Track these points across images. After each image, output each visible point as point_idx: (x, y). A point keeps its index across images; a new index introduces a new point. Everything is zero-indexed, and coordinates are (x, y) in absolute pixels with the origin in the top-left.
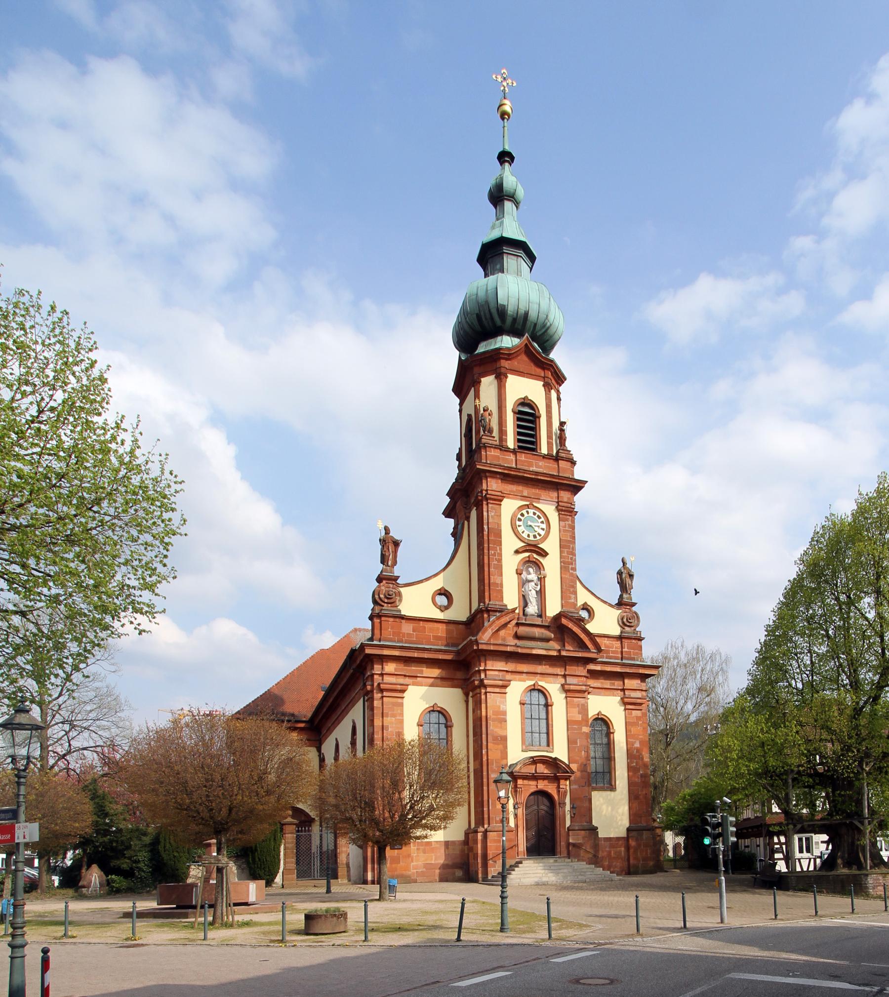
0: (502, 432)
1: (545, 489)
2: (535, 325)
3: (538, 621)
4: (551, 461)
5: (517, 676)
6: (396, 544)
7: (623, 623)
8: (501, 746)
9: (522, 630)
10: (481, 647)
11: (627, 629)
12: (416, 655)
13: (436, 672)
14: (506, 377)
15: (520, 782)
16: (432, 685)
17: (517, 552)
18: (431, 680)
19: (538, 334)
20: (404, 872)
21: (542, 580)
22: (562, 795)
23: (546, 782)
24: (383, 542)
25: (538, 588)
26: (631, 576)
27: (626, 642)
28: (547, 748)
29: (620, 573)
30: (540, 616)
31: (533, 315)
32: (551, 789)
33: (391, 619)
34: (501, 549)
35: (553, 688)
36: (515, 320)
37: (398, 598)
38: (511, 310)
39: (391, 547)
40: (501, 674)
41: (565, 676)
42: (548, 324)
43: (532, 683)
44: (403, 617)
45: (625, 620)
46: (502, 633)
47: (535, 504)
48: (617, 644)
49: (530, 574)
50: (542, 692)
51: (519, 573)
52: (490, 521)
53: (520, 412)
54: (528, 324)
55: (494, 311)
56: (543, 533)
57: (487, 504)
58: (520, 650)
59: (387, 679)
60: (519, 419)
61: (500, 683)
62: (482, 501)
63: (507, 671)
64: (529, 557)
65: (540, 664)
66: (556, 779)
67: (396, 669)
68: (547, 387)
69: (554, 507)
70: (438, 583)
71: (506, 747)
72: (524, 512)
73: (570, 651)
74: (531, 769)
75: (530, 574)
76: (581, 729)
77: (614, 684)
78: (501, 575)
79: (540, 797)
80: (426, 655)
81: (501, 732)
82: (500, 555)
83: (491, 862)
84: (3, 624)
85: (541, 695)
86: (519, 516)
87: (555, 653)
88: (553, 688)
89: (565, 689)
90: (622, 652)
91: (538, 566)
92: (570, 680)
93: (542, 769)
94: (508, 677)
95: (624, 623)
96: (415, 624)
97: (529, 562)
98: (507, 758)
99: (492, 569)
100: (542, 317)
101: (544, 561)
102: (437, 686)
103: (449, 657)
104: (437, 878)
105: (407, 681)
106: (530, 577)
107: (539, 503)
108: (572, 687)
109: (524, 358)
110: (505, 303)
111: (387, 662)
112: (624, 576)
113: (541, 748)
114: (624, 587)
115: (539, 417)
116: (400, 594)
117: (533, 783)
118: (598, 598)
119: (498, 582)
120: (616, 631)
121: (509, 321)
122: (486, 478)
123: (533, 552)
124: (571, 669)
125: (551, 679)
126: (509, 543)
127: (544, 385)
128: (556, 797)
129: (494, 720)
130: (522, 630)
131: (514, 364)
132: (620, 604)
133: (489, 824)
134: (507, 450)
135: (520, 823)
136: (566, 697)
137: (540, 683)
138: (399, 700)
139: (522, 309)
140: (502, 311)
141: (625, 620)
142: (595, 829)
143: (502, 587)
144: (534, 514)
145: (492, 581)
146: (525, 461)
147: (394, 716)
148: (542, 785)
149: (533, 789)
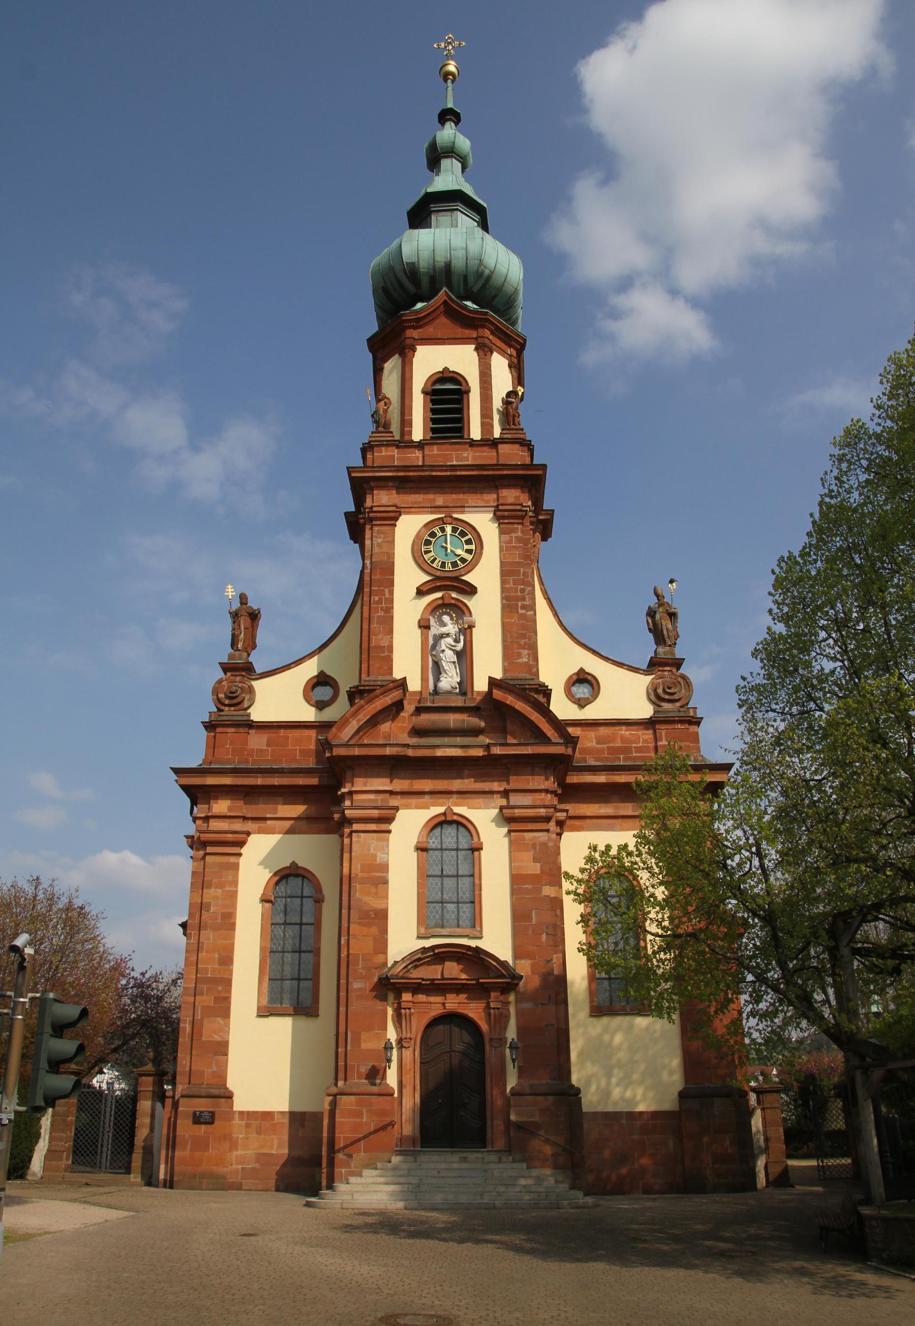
0: (406, 423)
2: (465, 277)
3: (459, 702)
4: (486, 449)
5: (414, 801)
6: (254, 616)
8: (374, 930)
9: (426, 719)
10: (337, 752)
11: (666, 706)
12: (259, 781)
13: (298, 810)
14: (414, 350)
15: (406, 997)
16: (290, 831)
17: (421, 592)
19: (475, 289)
20: (214, 1168)
21: (467, 631)
22: (500, 1021)
23: (462, 997)
24: (235, 616)
25: (460, 646)
26: (672, 616)
27: (663, 730)
28: (468, 931)
29: (651, 613)
31: (458, 264)
32: (474, 1010)
33: (232, 730)
35: (483, 817)
38: (423, 265)
39: (244, 622)
40: (380, 797)
41: (506, 794)
42: (487, 272)
43: (441, 810)
44: (251, 725)
45: (660, 691)
46: (385, 727)
47: (455, 516)
48: (648, 735)
49: (444, 625)
50: (462, 824)
51: (424, 626)
52: (376, 550)
53: (435, 392)
54: (455, 279)
55: (401, 275)
56: (469, 557)
57: (372, 529)
58: (410, 753)
59: (215, 825)
60: (434, 402)
61: (375, 813)
62: (364, 525)
63: (391, 793)
64: (442, 598)
65: (460, 777)
66: (477, 991)
67: (230, 809)
68: (484, 350)
70: (310, 669)
71: (384, 930)
72: (436, 529)
74: (432, 972)
75: (444, 625)
76: (540, 890)
78: (391, 632)
79: (456, 1030)
80: (276, 781)
81: (376, 904)
82: (391, 601)
83: (340, 1156)
84: (914, 911)
87: (480, 753)
88: (483, 817)
91: (459, 611)
92: (515, 799)
93: (453, 970)
94: (394, 802)
95: (656, 697)
96: (272, 734)
97: (438, 608)
98: (384, 951)
99: (374, 626)
100: (473, 263)
101: (472, 603)
102: (299, 833)
103: (314, 781)
104: (272, 1183)
105: (249, 826)
106: (444, 630)
107: (463, 512)
108: (517, 812)
109: (444, 320)
110: (414, 260)
111: (216, 798)
112: (658, 616)
113: (458, 931)
114: (659, 636)
115: (468, 392)
116: (251, 690)
117: (439, 999)
118: (607, 659)
119: (384, 643)
120: (646, 711)
122: (372, 489)
123: (449, 590)
124: (516, 782)
125: (480, 801)
127: (476, 349)
128: (484, 1026)
129: (363, 881)
130: (426, 719)
131: (430, 330)
132: (654, 665)
133: (345, 1080)
135: (407, 1078)
136: (509, 831)
137: (457, 810)
138: (233, 859)
139: (441, 259)
140: (412, 271)
141: (660, 691)
142: (575, 1093)
144: (454, 530)
145: (373, 644)
146: (438, 455)
147: (220, 886)
148: (454, 1003)
149: (436, 1011)
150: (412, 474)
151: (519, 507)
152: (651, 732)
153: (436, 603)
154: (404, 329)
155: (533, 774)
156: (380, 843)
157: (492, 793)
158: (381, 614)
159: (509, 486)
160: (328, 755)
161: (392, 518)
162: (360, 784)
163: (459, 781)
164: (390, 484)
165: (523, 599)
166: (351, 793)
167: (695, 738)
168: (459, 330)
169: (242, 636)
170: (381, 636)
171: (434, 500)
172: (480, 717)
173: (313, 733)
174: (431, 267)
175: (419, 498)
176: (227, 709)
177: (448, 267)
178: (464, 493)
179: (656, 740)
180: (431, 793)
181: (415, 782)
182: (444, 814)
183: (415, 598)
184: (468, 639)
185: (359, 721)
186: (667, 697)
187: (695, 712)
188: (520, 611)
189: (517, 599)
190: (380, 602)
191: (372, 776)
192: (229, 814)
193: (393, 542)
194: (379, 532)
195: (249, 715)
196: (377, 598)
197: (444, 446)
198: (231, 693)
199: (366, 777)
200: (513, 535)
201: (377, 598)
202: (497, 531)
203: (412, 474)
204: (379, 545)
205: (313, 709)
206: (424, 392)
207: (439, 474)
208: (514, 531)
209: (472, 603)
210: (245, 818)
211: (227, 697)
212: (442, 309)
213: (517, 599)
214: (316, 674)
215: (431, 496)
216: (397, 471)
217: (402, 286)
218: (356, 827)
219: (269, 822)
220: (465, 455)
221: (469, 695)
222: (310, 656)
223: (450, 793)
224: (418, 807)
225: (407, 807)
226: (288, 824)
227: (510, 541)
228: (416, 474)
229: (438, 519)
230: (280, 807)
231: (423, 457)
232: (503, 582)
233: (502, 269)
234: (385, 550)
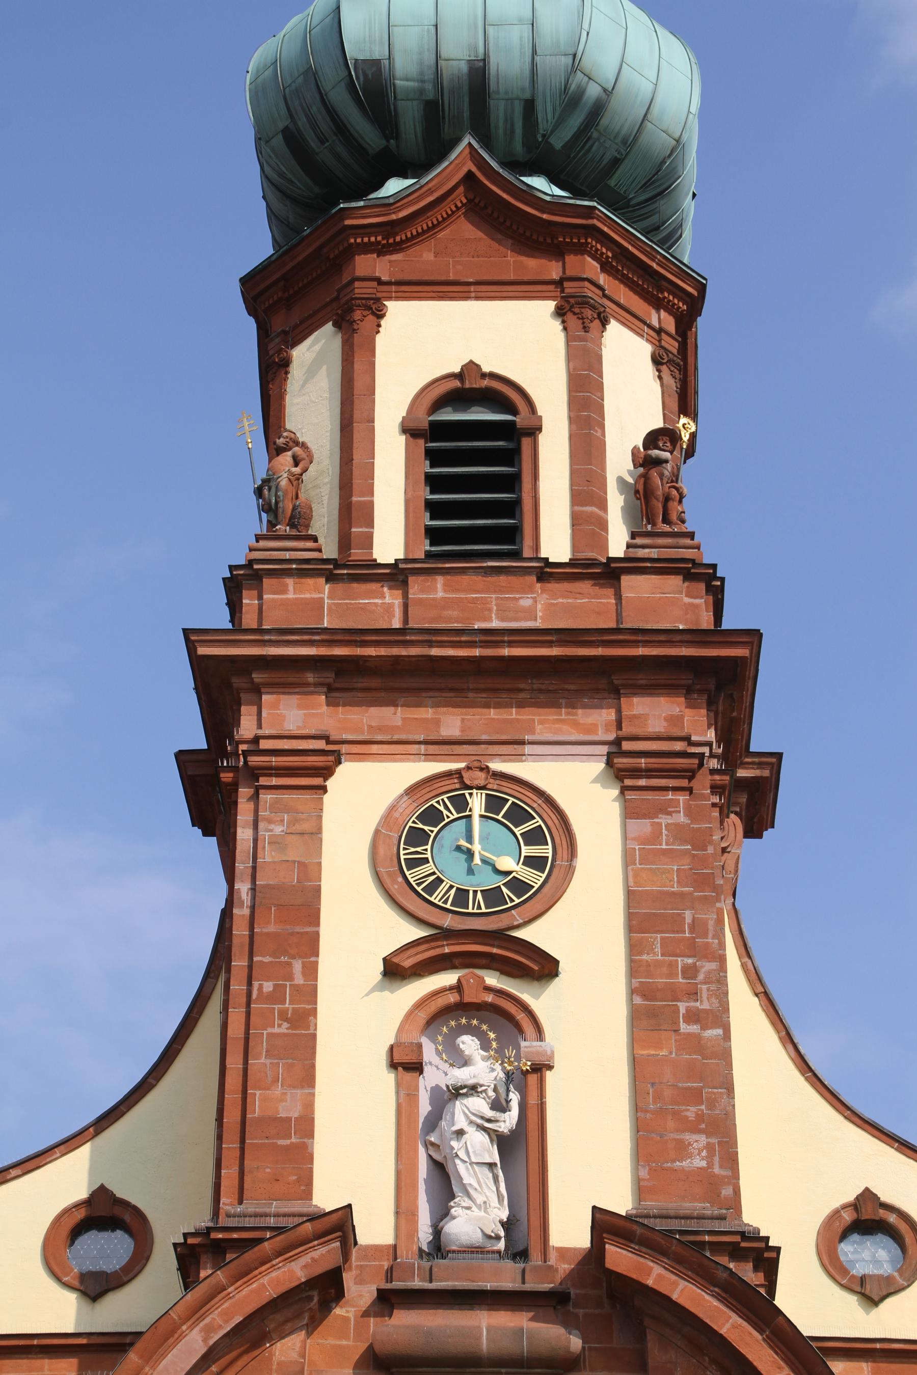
0: (354, 512)
2: (529, 106)
3: (506, 1277)
4: (586, 586)
14: (379, 314)
17: (394, 971)
19: (558, 142)
21: (530, 1077)
31: (509, 65)
34: (311, 971)
36: (433, 110)
38: (407, 66)
42: (593, 91)
47: (496, 766)
49: (465, 1062)
51: (404, 1063)
52: (267, 855)
53: (438, 430)
57: (255, 797)
62: (234, 787)
64: (458, 987)
68: (581, 315)
69: (599, 766)
70: (67, 1182)
78: (308, 1078)
91: (506, 1022)
99: (260, 1062)
100: (553, 65)
101: (543, 1001)
109: (465, 230)
110: (379, 52)
115: (534, 431)
119: (289, 1109)
121: (410, 118)
122: (257, 691)
123: (479, 965)
127: (560, 312)
131: (423, 258)
139: (458, 51)
140: (371, 85)
144: (494, 804)
145: (256, 1110)
150: (371, 651)
153: (441, 1002)
154: (349, 253)
158: (284, 1028)
161: (314, 769)
164: (310, 677)
165: (694, 994)
168: (511, 258)
170: (278, 1090)
171: (437, 723)
174: (429, 75)
177: (479, 74)
178: (521, 705)
183: (378, 988)
184: (533, 1100)
188: (684, 1027)
189: (674, 994)
190: (277, 996)
194: (276, 807)
196: (268, 987)
197: (465, 579)
200: (664, 820)
201: (268, 987)
202: (615, 810)
203: (371, 651)
204: (275, 842)
206: (409, 430)
208: (665, 809)
209: (543, 1001)
212: (460, 197)
213: (674, 994)
214: (83, 1194)
215: (427, 713)
216: (330, 643)
217: (341, 127)
221: (536, 1259)
227: (655, 837)
229: (448, 774)
231: (406, 607)
232: (634, 948)
233: (638, 83)
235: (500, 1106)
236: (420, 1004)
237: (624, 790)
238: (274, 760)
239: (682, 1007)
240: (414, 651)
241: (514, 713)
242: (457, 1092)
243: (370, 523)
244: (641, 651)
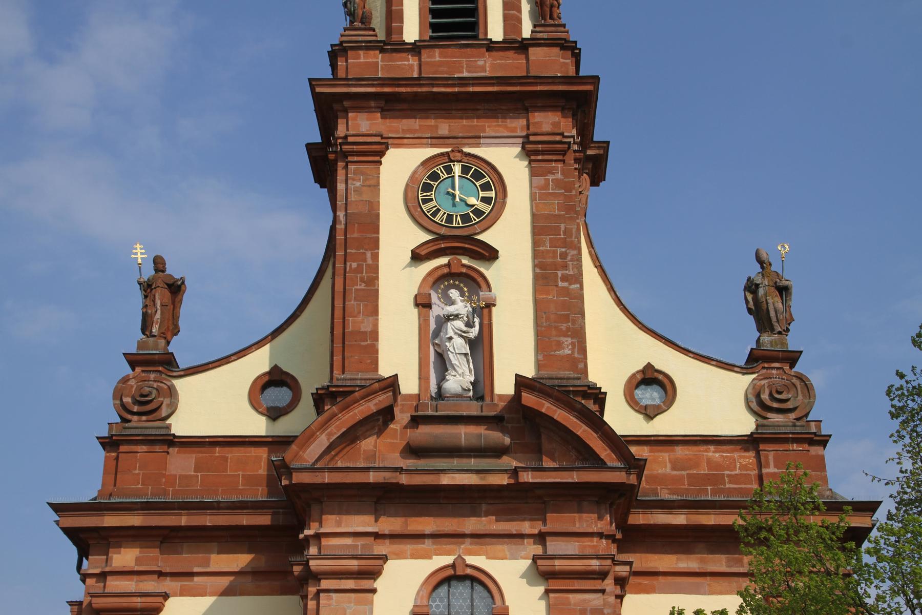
1: (493, 114)
3: (473, 409)
4: (511, 54)
5: (409, 547)
6: (176, 288)
7: (761, 404)
10: (297, 478)
11: (774, 418)
13: (240, 561)
17: (417, 257)
18: (225, 581)
24: (147, 288)
25: (474, 332)
26: (783, 291)
27: (770, 452)
29: (751, 287)
30: (479, 398)
34: (376, 257)
35: (509, 571)
37: (166, 401)
39: (161, 296)
40: (360, 542)
41: (541, 538)
43: (448, 560)
44: (172, 441)
45: (765, 396)
46: (368, 444)
47: (466, 150)
48: (749, 458)
49: (452, 303)
50: (478, 580)
51: (423, 304)
52: (353, 197)
57: (346, 167)
58: (404, 479)
61: (353, 564)
62: (335, 162)
63: (377, 536)
64: (448, 265)
65: (475, 513)
67: (138, 560)
70: (259, 363)
73: (553, 472)
75: (452, 303)
77: (740, 562)
78: (375, 312)
80: (208, 520)
82: (375, 269)
85: (478, 588)
86: (492, 194)
89: (546, 574)
90: (760, 478)
91: (473, 283)
92: (555, 546)
94: (380, 548)
95: (759, 405)
97: (443, 280)
99: (351, 303)
101: (491, 272)
102: (242, 594)
103: (264, 520)
107: (478, 145)
108: (559, 564)
111: (119, 546)
112: (761, 292)
114: (762, 318)
116: (172, 392)
119: (366, 327)
122: (346, 111)
123: (458, 253)
124: (556, 521)
125: (503, 547)
126: (398, 235)
132: (756, 360)
134: (402, 48)
136: (547, 592)
137: (471, 560)
141: (765, 396)
143: (376, 338)
144: (465, 170)
145: (350, 328)
150: (403, 90)
151: (558, 138)
152: (752, 454)
153: (440, 273)
155: (580, 511)
156: (362, 608)
157: (521, 536)
158: (363, 286)
159: (544, 108)
160: (285, 482)
162: (330, 524)
163: (473, 520)
164: (373, 104)
165: (565, 267)
166: (318, 536)
167: (820, 465)
169: (158, 316)
170: (361, 318)
171: (436, 127)
172: (504, 431)
173: (262, 453)
175: (413, 124)
176: (135, 418)
178: (478, 117)
179: (760, 466)
180: (434, 536)
181: (411, 520)
182: (453, 566)
183: (409, 265)
185: (330, 434)
186: (775, 405)
187: (819, 427)
188: (560, 284)
189: (556, 267)
190: (359, 270)
191: (348, 513)
192: (137, 568)
193: (377, 185)
194: (356, 172)
195: (168, 427)
196: (354, 265)
197: (450, 51)
198: (142, 396)
199: (340, 513)
200: (550, 177)
201: (354, 265)
203: (403, 90)
204: (356, 190)
205: (264, 419)
207: (443, 90)
208: (551, 171)
209: (491, 272)
210: (161, 574)
211: (136, 402)
213: (556, 267)
214: (266, 368)
215: (432, 122)
216: (382, 85)
218: (325, 584)
219: (196, 579)
220: (481, 63)
221: (488, 400)
222: (259, 344)
223: (463, 536)
224: (415, 556)
225: (400, 556)
226: (225, 581)
227: (546, 186)
228: (409, 90)
229: (442, 154)
230: (214, 557)
232: (535, 244)
234: (365, 197)
235: (470, 325)
236: (430, 274)
237: (530, 162)
238: (355, 148)
239: (560, 273)
240: (424, 89)
241: (475, 122)
242: (449, 318)
243: (402, 21)
244: (539, 88)
